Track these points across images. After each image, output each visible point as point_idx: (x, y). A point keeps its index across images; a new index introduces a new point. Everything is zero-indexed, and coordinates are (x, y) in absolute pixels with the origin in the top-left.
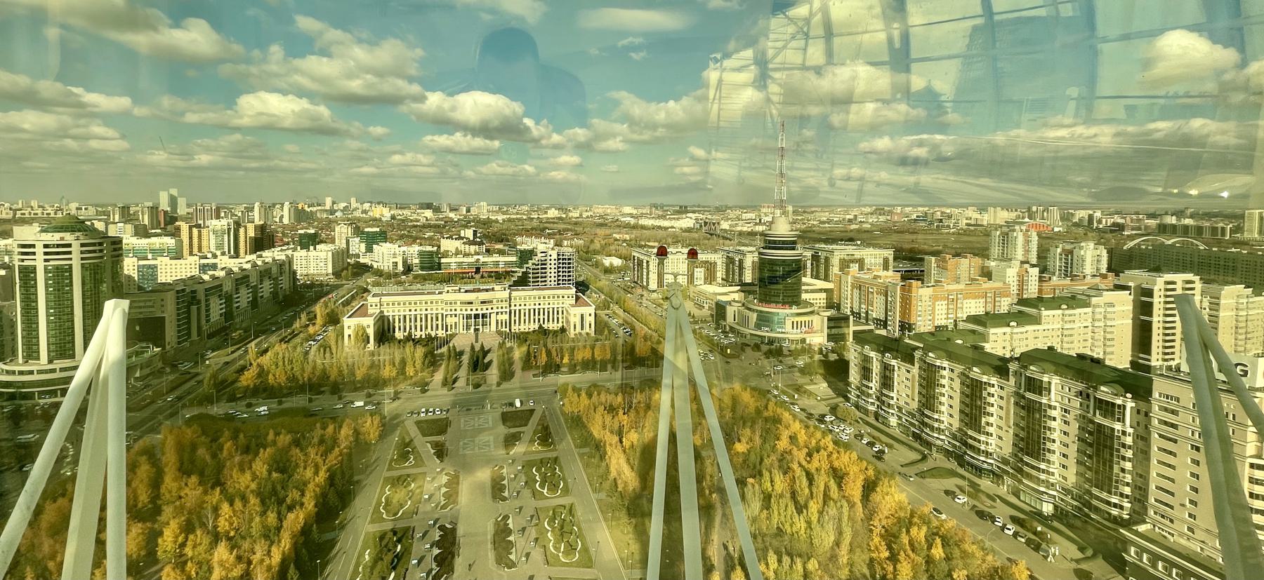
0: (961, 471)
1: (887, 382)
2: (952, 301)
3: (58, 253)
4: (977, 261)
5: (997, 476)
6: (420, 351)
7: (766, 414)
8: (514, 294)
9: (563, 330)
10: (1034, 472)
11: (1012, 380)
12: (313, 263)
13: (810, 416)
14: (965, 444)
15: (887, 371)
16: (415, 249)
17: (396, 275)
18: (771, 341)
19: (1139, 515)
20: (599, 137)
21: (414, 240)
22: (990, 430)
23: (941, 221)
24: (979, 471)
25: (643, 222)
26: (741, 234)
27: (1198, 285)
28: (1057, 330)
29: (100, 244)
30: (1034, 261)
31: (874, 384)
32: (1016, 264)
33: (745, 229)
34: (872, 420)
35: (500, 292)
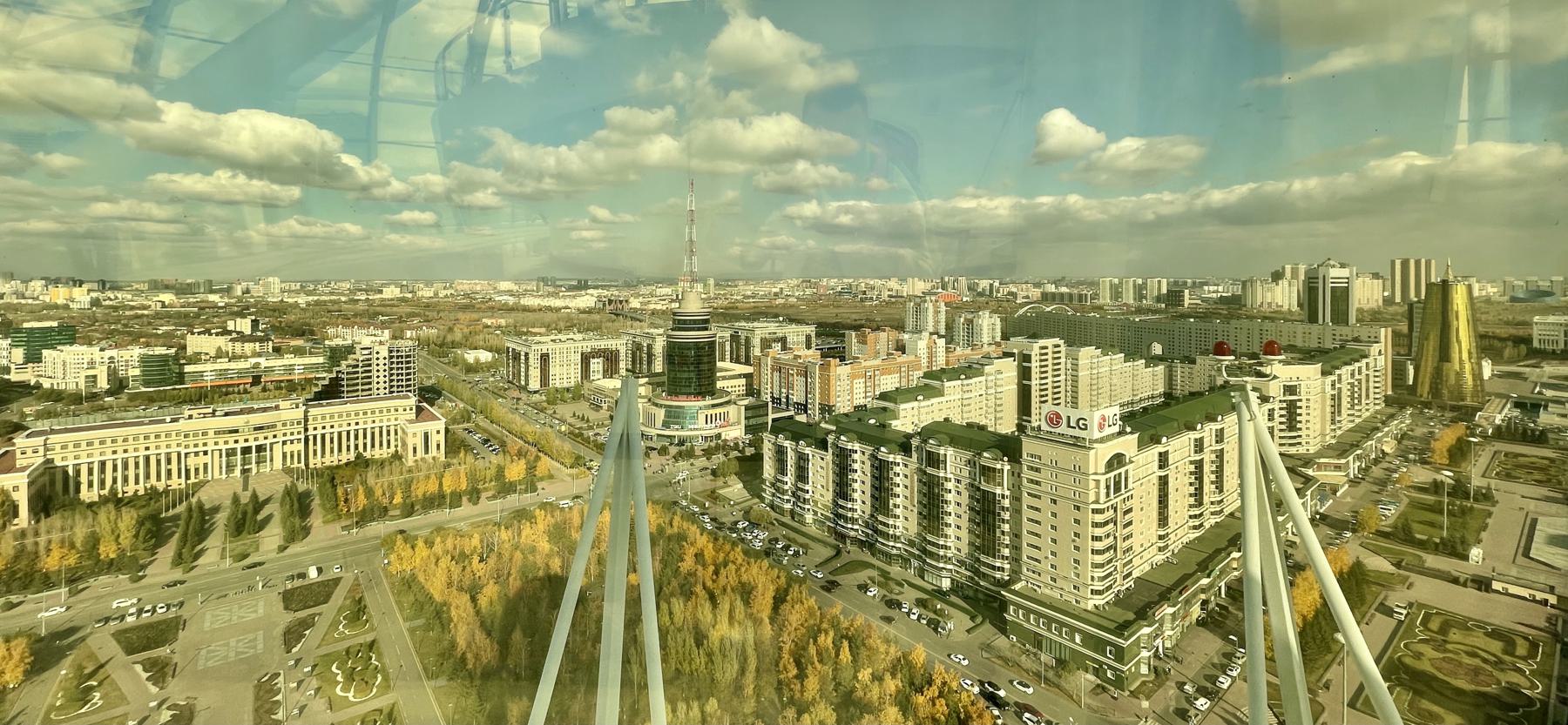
0: (874, 561)
1: (802, 475)
2: (869, 378)
4: (894, 334)
5: (905, 561)
6: (128, 519)
7: (669, 531)
8: (313, 411)
9: (397, 457)
10: (934, 549)
11: (915, 455)
13: (720, 526)
14: (876, 531)
15: (802, 459)
16: (136, 352)
17: (93, 397)
18: (681, 443)
19: (1016, 575)
20: (468, 186)
21: (135, 339)
24: (889, 558)
26: (653, 313)
27: (1063, 348)
28: (957, 403)
30: (943, 332)
31: (789, 479)
32: (925, 335)
33: (659, 307)
34: (787, 520)
35: (289, 411)
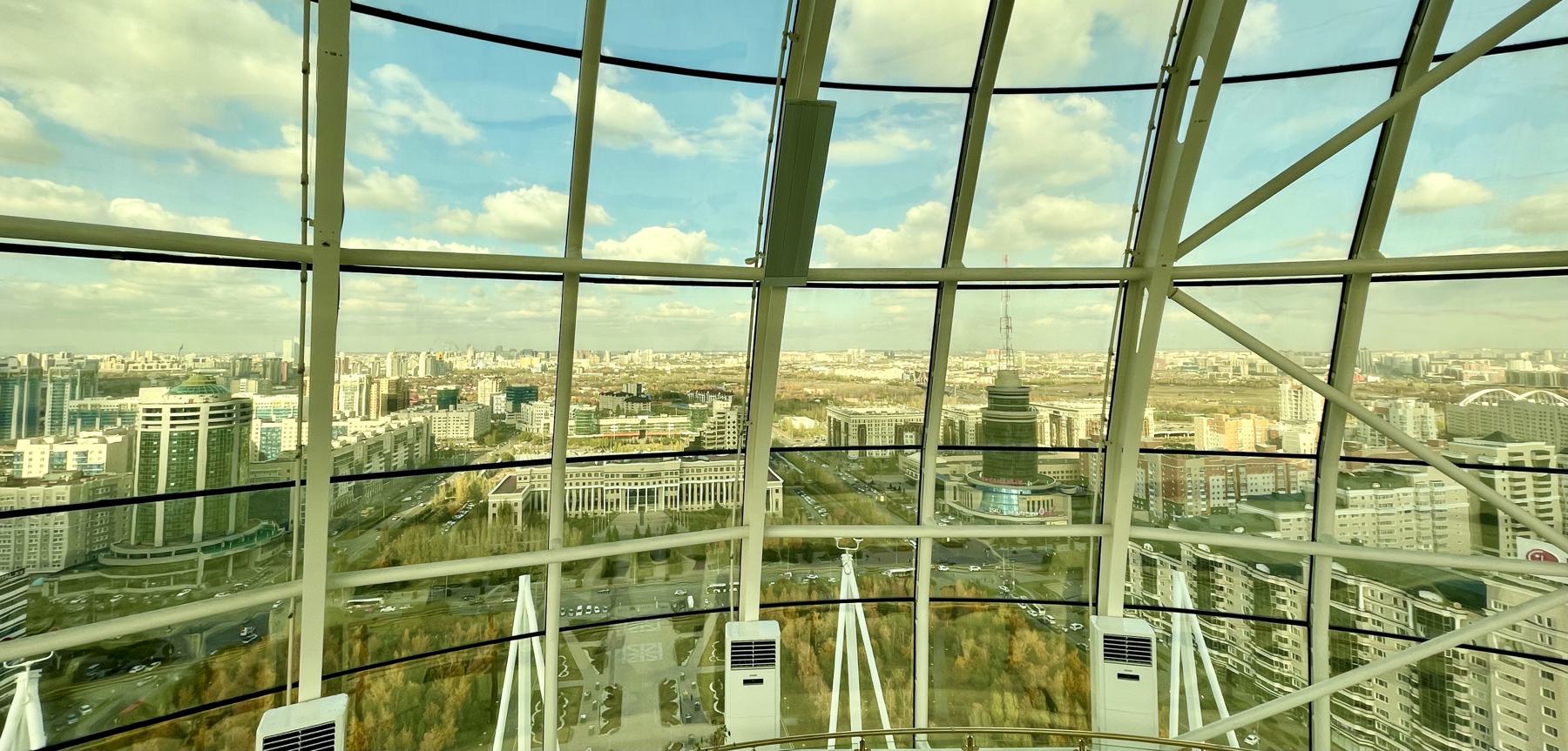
3: (185, 418)
12: (455, 429)
22: (1284, 647)
23: (1216, 369)
25: (839, 372)
29: (230, 407)
33: (966, 380)
